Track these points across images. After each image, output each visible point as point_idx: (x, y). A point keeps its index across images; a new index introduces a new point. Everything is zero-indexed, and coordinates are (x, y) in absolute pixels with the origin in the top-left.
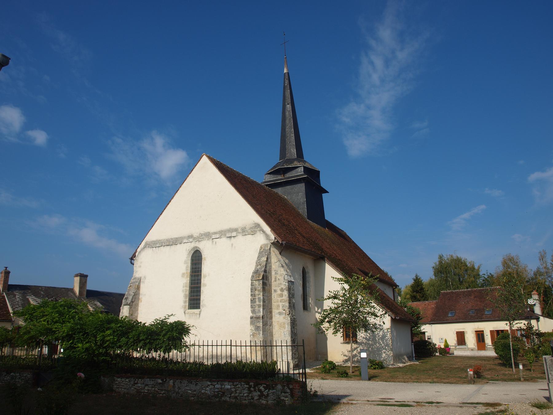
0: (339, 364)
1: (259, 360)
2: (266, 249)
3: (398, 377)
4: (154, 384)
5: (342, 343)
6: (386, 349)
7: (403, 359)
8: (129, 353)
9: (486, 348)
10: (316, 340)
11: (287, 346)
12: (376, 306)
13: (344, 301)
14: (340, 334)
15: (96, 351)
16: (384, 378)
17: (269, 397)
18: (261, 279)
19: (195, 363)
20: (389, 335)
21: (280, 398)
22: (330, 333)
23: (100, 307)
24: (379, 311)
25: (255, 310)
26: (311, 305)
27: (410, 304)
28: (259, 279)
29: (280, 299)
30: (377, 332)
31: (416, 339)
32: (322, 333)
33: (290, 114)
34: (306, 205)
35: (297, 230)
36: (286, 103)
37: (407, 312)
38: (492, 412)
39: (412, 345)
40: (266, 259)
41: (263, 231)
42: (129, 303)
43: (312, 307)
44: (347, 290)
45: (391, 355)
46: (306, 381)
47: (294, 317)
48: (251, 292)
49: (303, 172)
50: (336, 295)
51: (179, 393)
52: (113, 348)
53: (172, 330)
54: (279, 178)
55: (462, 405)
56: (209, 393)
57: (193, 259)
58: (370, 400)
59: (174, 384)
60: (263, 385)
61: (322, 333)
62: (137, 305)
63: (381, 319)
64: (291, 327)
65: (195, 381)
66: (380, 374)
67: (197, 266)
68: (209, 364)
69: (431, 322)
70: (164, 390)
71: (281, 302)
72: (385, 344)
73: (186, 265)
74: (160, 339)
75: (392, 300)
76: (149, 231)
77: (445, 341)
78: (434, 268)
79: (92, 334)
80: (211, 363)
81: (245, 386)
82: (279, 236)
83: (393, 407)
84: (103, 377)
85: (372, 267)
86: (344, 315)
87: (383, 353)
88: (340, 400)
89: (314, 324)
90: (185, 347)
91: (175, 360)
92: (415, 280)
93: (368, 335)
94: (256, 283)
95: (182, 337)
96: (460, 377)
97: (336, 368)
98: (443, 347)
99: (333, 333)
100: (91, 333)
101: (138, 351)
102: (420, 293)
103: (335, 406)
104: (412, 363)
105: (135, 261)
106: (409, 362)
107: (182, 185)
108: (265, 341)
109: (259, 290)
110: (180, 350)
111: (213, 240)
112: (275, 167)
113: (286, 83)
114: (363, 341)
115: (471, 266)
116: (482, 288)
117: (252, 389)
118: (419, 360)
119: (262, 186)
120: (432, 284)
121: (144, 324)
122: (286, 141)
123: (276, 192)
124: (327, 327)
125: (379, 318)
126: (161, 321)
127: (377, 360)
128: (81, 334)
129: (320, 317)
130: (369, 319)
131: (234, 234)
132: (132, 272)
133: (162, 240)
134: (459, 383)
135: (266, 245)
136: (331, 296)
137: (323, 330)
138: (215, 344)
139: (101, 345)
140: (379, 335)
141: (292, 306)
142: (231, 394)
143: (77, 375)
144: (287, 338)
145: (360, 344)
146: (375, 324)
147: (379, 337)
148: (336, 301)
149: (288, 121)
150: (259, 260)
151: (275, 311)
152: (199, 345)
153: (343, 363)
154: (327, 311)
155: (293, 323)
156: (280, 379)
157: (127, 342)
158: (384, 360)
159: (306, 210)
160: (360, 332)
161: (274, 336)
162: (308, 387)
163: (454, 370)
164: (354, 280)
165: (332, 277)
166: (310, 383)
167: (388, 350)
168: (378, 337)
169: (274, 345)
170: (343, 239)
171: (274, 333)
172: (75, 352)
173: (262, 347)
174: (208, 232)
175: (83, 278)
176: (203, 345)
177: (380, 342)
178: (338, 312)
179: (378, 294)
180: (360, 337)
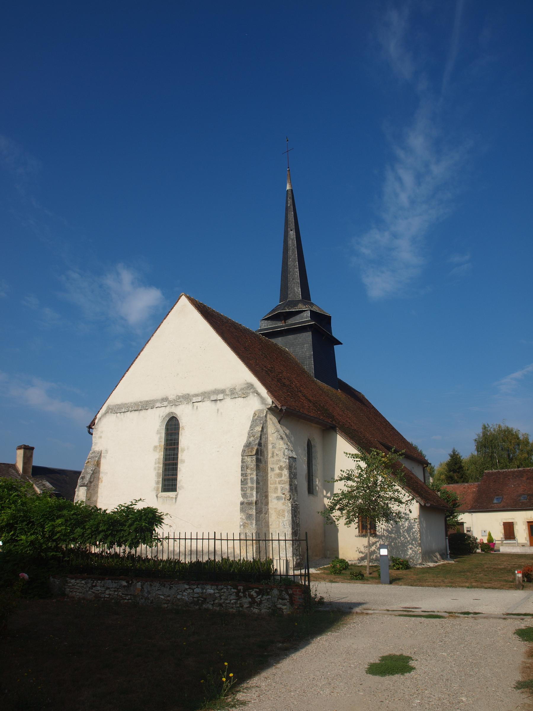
0: (353, 563)
1: (250, 559)
2: (261, 416)
4: (117, 587)
8: (86, 547)
11: (285, 540)
12: (400, 489)
13: (360, 483)
14: (354, 525)
16: (410, 581)
17: (263, 605)
18: (254, 454)
19: (169, 561)
20: (416, 527)
21: (276, 606)
22: (341, 523)
24: (404, 495)
25: (246, 493)
28: (251, 454)
29: (278, 480)
31: (451, 531)
32: (331, 523)
33: (294, 242)
34: (313, 359)
35: (300, 391)
36: (289, 229)
37: (440, 498)
40: (260, 429)
41: (257, 394)
42: (86, 484)
44: (363, 469)
46: (309, 585)
48: (242, 470)
49: (309, 317)
53: (141, 519)
54: (280, 325)
56: (187, 599)
58: (390, 610)
59: (142, 588)
60: (255, 590)
61: (331, 523)
62: (97, 486)
63: (407, 506)
64: (292, 515)
65: (169, 583)
67: (173, 437)
68: (187, 563)
69: (472, 510)
70: (130, 595)
71: (279, 483)
73: (159, 435)
74: (125, 531)
75: (421, 481)
76: (112, 392)
78: (476, 440)
79: (39, 523)
80: (190, 562)
81: (232, 590)
82: (278, 400)
83: (419, 619)
86: (360, 501)
87: (409, 549)
90: (157, 541)
91: (144, 556)
92: (451, 456)
93: (390, 527)
94: (248, 459)
96: (507, 581)
97: (349, 567)
98: (485, 541)
99: (346, 524)
100: (37, 522)
102: (459, 472)
104: (446, 562)
105: (94, 430)
107: (154, 333)
110: (150, 544)
111: (194, 404)
112: (273, 310)
114: (383, 533)
118: (454, 559)
119: (257, 335)
120: (473, 461)
121: (105, 511)
123: (275, 343)
124: (338, 516)
125: (404, 505)
126: (126, 507)
128: (25, 523)
129: (330, 504)
130: (392, 506)
131: (220, 396)
133: (129, 403)
134: (504, 588)
135: (261, 411)
136: (343, 476)
137: (333, 519)
141: (293, 489)
143: (19, 576)
144: (288, 531)
145: (380, 537)
146: (399, 512)
147: (404, 529)
148: (350, 483)
150: (252, 430)
151: (272, 495)
152: (174, 539)
153: (358, 561)
154: (338, 496)
155: (295, 510)
156: (276, 582)
157: (83, 534)
158: (410, 558)
159: (313, 366)
160: (380, 523)
161: (270, 526)
163: (498, 571)
165: (344, 453)
166: (314, 588)
167: (415, 546)
168: (403, 528)
171: (270, 523)
174: (187, 394)
175: (28, 451)
177: (405, 536)
178: (352, 497)
179: (403, 474)
180: (380, 529)
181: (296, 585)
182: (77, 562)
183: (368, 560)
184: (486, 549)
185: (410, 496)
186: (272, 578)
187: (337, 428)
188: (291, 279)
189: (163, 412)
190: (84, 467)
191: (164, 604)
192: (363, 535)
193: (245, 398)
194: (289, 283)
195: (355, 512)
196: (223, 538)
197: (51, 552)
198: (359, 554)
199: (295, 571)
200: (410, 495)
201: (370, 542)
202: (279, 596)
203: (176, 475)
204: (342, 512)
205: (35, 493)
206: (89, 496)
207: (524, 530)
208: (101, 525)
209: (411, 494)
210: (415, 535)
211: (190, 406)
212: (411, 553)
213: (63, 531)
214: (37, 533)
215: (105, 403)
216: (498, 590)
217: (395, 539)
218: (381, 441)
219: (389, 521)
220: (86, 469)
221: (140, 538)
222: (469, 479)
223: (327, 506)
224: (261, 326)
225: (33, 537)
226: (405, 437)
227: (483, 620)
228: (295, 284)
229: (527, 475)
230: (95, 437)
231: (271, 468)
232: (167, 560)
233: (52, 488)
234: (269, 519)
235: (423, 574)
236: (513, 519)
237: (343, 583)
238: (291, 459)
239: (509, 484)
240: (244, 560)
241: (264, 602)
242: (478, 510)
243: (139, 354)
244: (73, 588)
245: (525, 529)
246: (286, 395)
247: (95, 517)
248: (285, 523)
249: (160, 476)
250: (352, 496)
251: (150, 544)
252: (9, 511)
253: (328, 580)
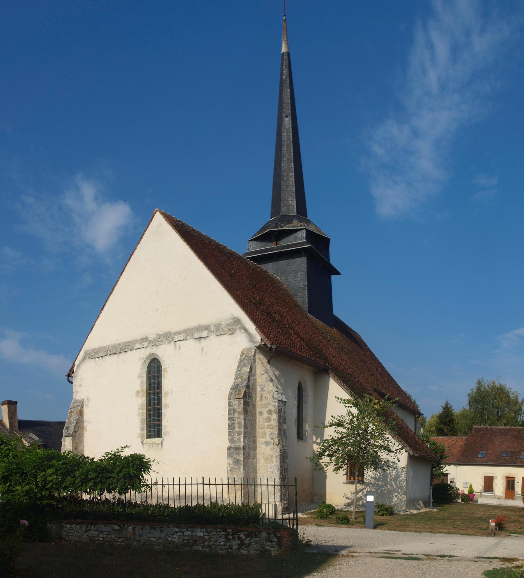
0: (340, 508)
1: (239, 502)
2: (249, 355)
3: (409, 525)
4: (110, 531)
5: (345, 484)
6: (399, 492)
7: (418, 504)
8: (78, 495)
9: (514, 497)
10: (313, 478)
11: (274, 485)
12: (390, 438)
13: (351, 430)
14: (342, 472)
15: (38, 494)
16: (393, 526)
17: (251, 547)
18: (242, 397)
19: (158, 506)
20: (403, 476)
21: (264, 548)
22: (330, 470)
23: (36, 441)
24: (394, 444)
25: (234, 438)
26: (308, 433)
27: (435, 438)
28: (239, 397)
29: (266, 424)
30: (389, 470)
31: (436, 482)
32: (320, 469)
33: (290, 135)
34: (307, 291)
35: (292, 328)
36: (284, 114)
37: (429, 449)
38: (508, 568)
39: (430, 488)
40: (248, 370)
41: (244, 330)
42: (71, 434)
43: (309, 435)
44: (355, 415)
45: (403, 500)
46: (297, 529)
47: (285, 447)
48: (229, 414)
49: (305, 239)
50: (340, 421)
51: (140, 541)
52: (57, 489)
53: (128, 466)
54: (270, 247)
55: (478, 559)
56: (178, 541)
57: (149, 371)
58: (373, 552)
59: (134, 531)
60: (244, 532)
61: (320, 469)
62: (82, 435)
63: (395, 455)
64: (280, 460)
65: (160, 527)
66: (388, 522)
67: (156, 381)
68: (176, 507)
69: (457, 463)
70: (123, 538)
71: (268, 428)
72: (398, 486)
73: (141, 380)
74: (114, 478)
75: (412, 431)
76: (88, 335)
77: (470, 485)
78: (469, 395)
79: (32, 474)
80: (179, 506)
81: (221, 533)
82: (267, 338)
83: (399, 560)
84: (50, 523)
85: (392, 387)
86: (350, 448)
87: (395, 496)
88: (338, 551)
89: (310, 458)
90: (145, 487)
91: (133, 502)
92: (444, 409)
93: (377, 475)
94: (236, 403)
95: (140, 474)
96: (481, 529)
97: (336, 512)
98: (466, 492)
99: (334, 471)
100: (30, 473)
101: (88, 493)
102: (449, 425)
103: (331, 558)
104: (428, 510)
105: (73, 378)
106: (425, 508)
107: (128, 263)
108: (246, 478)
109: (239, 413)
110: (139, 490)
111: (176, 343)
112: (263, 228)
113: (285, 74)
114: (371, 481)
115: (514, 399)
116: (522, 427)
117: (230, 537)
118: (436, 507)
119: (244, 260)
120: (464, 415)
121: (93, 459)
122: (282, 184)
123: (264, 269)
124: (327, 462)
125: (393, 454)
126: (113, 455)
127: (387, 505)
128: (19, 475)
129: (319, 450)
130: (381, 454)
131: (205, 334)
132: (71, 393)
133: (106, 346)
134: (478, 535)
135: (249, 350)
136: (334, 422)
137: (322, 465)
138: (182, 482)
139: (43, 486)
140: (392, 474)
141: (282, 434)
142: (205, 542)
143: (20, 523)
144: (276, 475)
145: (368, 485)
146: (387, 460)
147: (391, 478)
148: (340, 429)
149: (285, 149)
150: (239, 371)
151: (260, 439)
152: (162, 484)
153: (344, 507)
154: (328, 442)
155: (283, 456)
156: (265, 525)
157: (74, 482)
158: (395, 505)
159: (307, 299)
160: (368, 470)
161: (258, 472)
162: (299, 535)
163: (475, 520)
164: (365, 403)
165: (336, 397)
166: (302, 531)
167: (401, 494)
168: (390, 477)
169: (258, 484)
170: (355, 345)
171: (258, 468)
172: (14, 496)
173: (242, 486)
174: (169, 332)
175: (11, 406)
176: (168, 484)
177: (392, 484)
178: (342, 444)
179: (395, 423)
180: (368, 476)
181: (285, 529)
182: (71, 508)
183: (355, 505)
184: (466, 499)
185: (400, 445)
186: (261, 522)
187: (330, 371)
188: (285, 187)
189: (144, 354)
190: (68, 418)
191: (156, 545)
192: (351, 482)
193: (231, 335)
194: (282, 192)
195: (344, 459)
196: (211, 483)
197: (46, 500)
198: (346, 500)
199: (283, 515)
200: (399, 444)
201: (358, 489)
202: (267, 539)
203: (161, 420)
204: (331, 458)
205: (24, 446)
206: (76, 446)
207: (502, 484)
208: (90, 473)
209: (400, 444)
210: (402, 484)
212: (396, 501)
213: (55, 480)
214: (31, 483)
215: (82, 349)
216: (472, 536)
217: (382, 486)
218: (375, 387)
219: (378, 469)
220: (69, 419)
221: (129, 484)
222: (458, 432)
223: (316, 452)
224: (249, 248)
225: (28, 487)
226: (399, 385)
227: (457, 562)
228: (290, 194)
229: (512, 433)
230: (76, 385)
231: (259, 412)
232: (156, 505)
233: (39, 440)
234: (256, 464)
235: (406, 520)
236: (494, 473)
237: (329, 526)
238: (280, 403)
239: (494, 441)
240: (232, 504)
241: (252, 544)
242: (463, 463)
243: (113, 289)
244: (69, 532)
245: (503, 483)
246: (276, 332)
247: (83, 465)
248: (273, 468)
249: (145, 422)
250: (342, 443)
251: (139, 490)
252: (3, 464)
253: (314, 524)
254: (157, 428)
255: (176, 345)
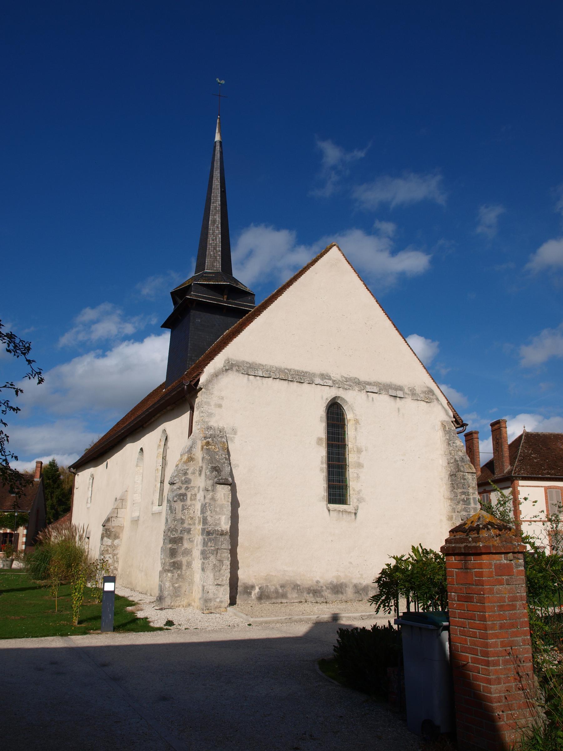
193: (428, 403)
211: (363, 395)
254: (340, 492)
255: (368, 396)
